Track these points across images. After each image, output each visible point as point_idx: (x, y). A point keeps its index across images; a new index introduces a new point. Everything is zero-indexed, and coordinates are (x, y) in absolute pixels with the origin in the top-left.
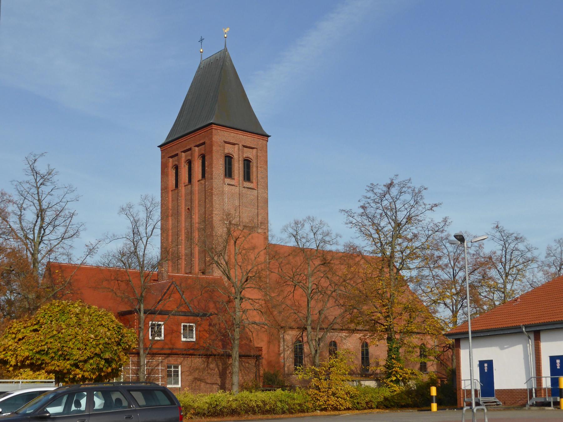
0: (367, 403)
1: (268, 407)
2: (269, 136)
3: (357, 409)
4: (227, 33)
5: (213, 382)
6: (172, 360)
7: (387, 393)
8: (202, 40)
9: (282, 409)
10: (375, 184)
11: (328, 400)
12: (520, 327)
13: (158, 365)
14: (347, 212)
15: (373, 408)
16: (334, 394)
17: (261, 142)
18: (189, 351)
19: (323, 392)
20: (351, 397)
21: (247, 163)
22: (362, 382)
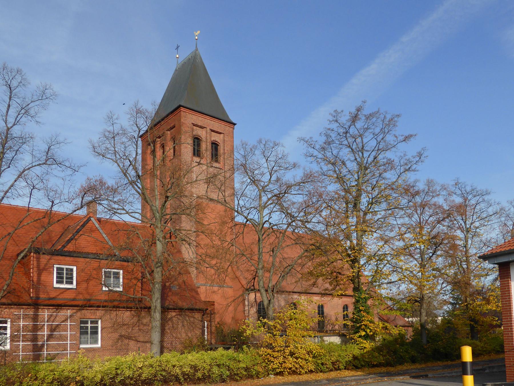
0: (333, 363)
1: (199, 375)
2: (235, 124)
3: (321, 372)
4: (198, 35)
5: (145, 340)
6: (88, 314)
7: (355, 350)
8: (178, 47)
9: (221, 376)
10: (339, 111)
11: (285, 362)
12: (344, 315)
13: (66, 320)
14: (307, 142)
15: (340, 370)
16: (292, 354)
17: (227, 128)
18: (114, 303)
19: (278, 351)
20: (314, 357)
21: (215, 145)
22: (325, 338)
